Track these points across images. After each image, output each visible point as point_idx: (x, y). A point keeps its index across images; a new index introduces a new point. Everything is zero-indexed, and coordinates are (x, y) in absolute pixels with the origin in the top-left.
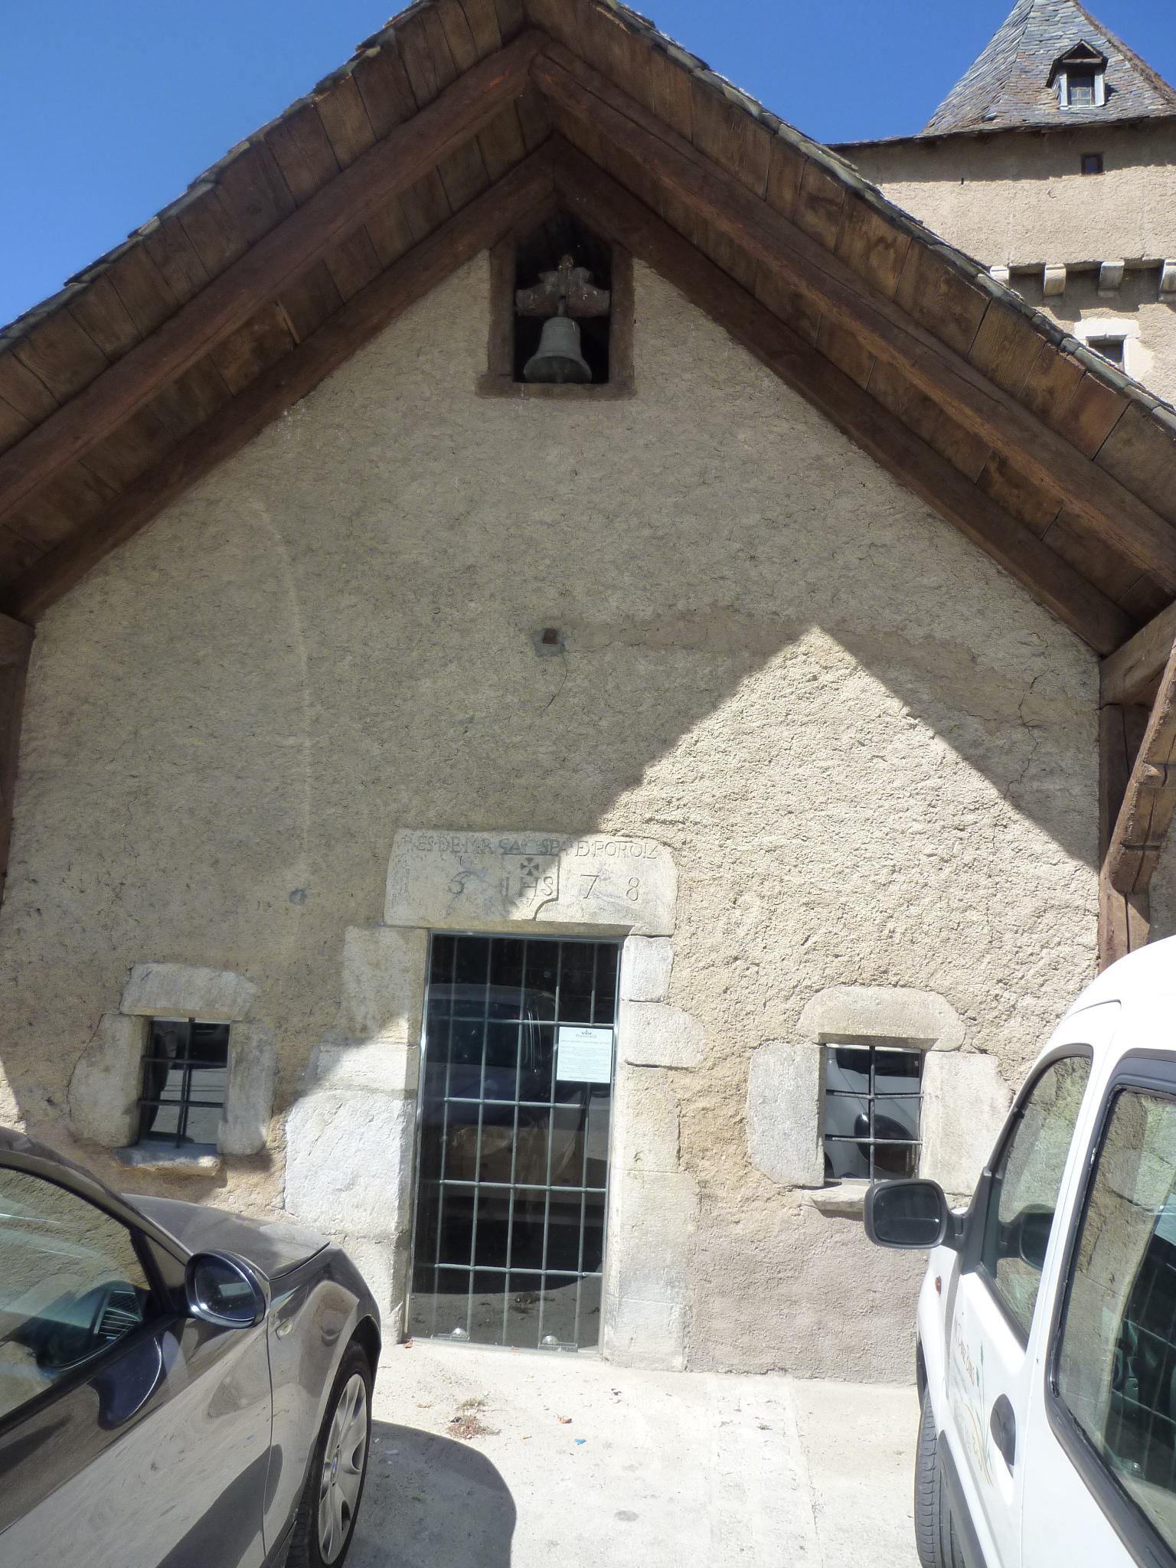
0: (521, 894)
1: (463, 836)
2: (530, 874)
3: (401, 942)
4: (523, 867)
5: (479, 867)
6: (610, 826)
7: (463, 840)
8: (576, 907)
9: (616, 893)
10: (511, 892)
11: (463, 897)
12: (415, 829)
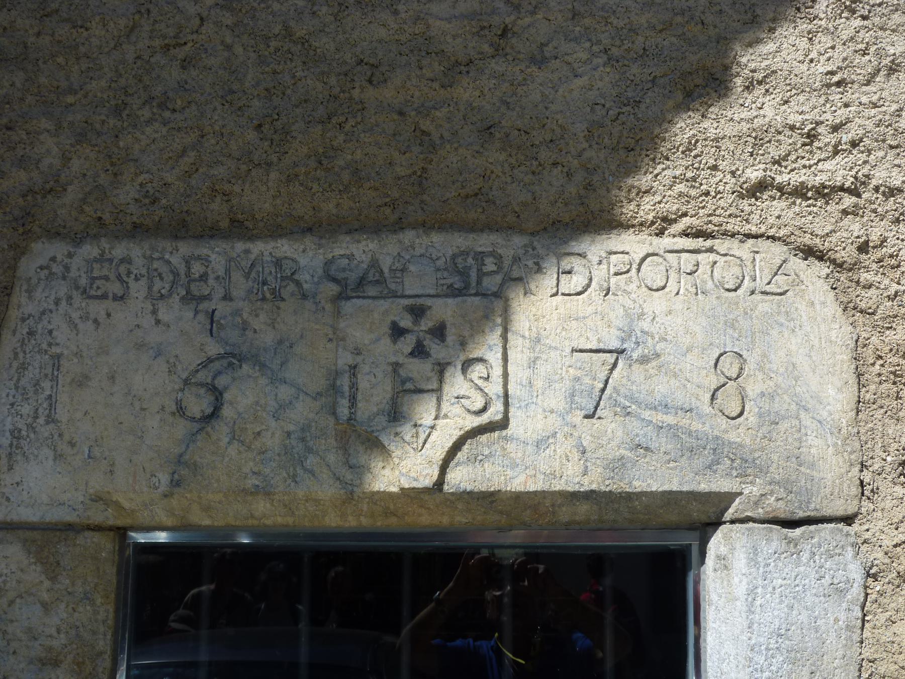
0: (396, 415)
1: (216, 254)
2: (419, 351)
3: (34, 574)
4: (397, 332)
5: (268, 338)
6: (647, 208)
7: (218, 263)
8: (563, 446)
9: (680, 398)
10: (365, 410)
11: (221, 431)
12: (77, 240)
